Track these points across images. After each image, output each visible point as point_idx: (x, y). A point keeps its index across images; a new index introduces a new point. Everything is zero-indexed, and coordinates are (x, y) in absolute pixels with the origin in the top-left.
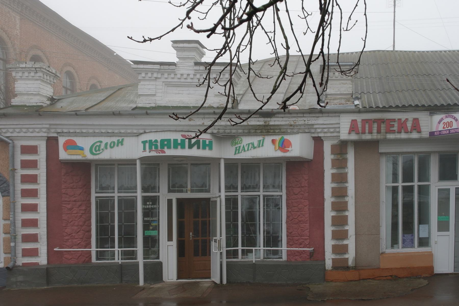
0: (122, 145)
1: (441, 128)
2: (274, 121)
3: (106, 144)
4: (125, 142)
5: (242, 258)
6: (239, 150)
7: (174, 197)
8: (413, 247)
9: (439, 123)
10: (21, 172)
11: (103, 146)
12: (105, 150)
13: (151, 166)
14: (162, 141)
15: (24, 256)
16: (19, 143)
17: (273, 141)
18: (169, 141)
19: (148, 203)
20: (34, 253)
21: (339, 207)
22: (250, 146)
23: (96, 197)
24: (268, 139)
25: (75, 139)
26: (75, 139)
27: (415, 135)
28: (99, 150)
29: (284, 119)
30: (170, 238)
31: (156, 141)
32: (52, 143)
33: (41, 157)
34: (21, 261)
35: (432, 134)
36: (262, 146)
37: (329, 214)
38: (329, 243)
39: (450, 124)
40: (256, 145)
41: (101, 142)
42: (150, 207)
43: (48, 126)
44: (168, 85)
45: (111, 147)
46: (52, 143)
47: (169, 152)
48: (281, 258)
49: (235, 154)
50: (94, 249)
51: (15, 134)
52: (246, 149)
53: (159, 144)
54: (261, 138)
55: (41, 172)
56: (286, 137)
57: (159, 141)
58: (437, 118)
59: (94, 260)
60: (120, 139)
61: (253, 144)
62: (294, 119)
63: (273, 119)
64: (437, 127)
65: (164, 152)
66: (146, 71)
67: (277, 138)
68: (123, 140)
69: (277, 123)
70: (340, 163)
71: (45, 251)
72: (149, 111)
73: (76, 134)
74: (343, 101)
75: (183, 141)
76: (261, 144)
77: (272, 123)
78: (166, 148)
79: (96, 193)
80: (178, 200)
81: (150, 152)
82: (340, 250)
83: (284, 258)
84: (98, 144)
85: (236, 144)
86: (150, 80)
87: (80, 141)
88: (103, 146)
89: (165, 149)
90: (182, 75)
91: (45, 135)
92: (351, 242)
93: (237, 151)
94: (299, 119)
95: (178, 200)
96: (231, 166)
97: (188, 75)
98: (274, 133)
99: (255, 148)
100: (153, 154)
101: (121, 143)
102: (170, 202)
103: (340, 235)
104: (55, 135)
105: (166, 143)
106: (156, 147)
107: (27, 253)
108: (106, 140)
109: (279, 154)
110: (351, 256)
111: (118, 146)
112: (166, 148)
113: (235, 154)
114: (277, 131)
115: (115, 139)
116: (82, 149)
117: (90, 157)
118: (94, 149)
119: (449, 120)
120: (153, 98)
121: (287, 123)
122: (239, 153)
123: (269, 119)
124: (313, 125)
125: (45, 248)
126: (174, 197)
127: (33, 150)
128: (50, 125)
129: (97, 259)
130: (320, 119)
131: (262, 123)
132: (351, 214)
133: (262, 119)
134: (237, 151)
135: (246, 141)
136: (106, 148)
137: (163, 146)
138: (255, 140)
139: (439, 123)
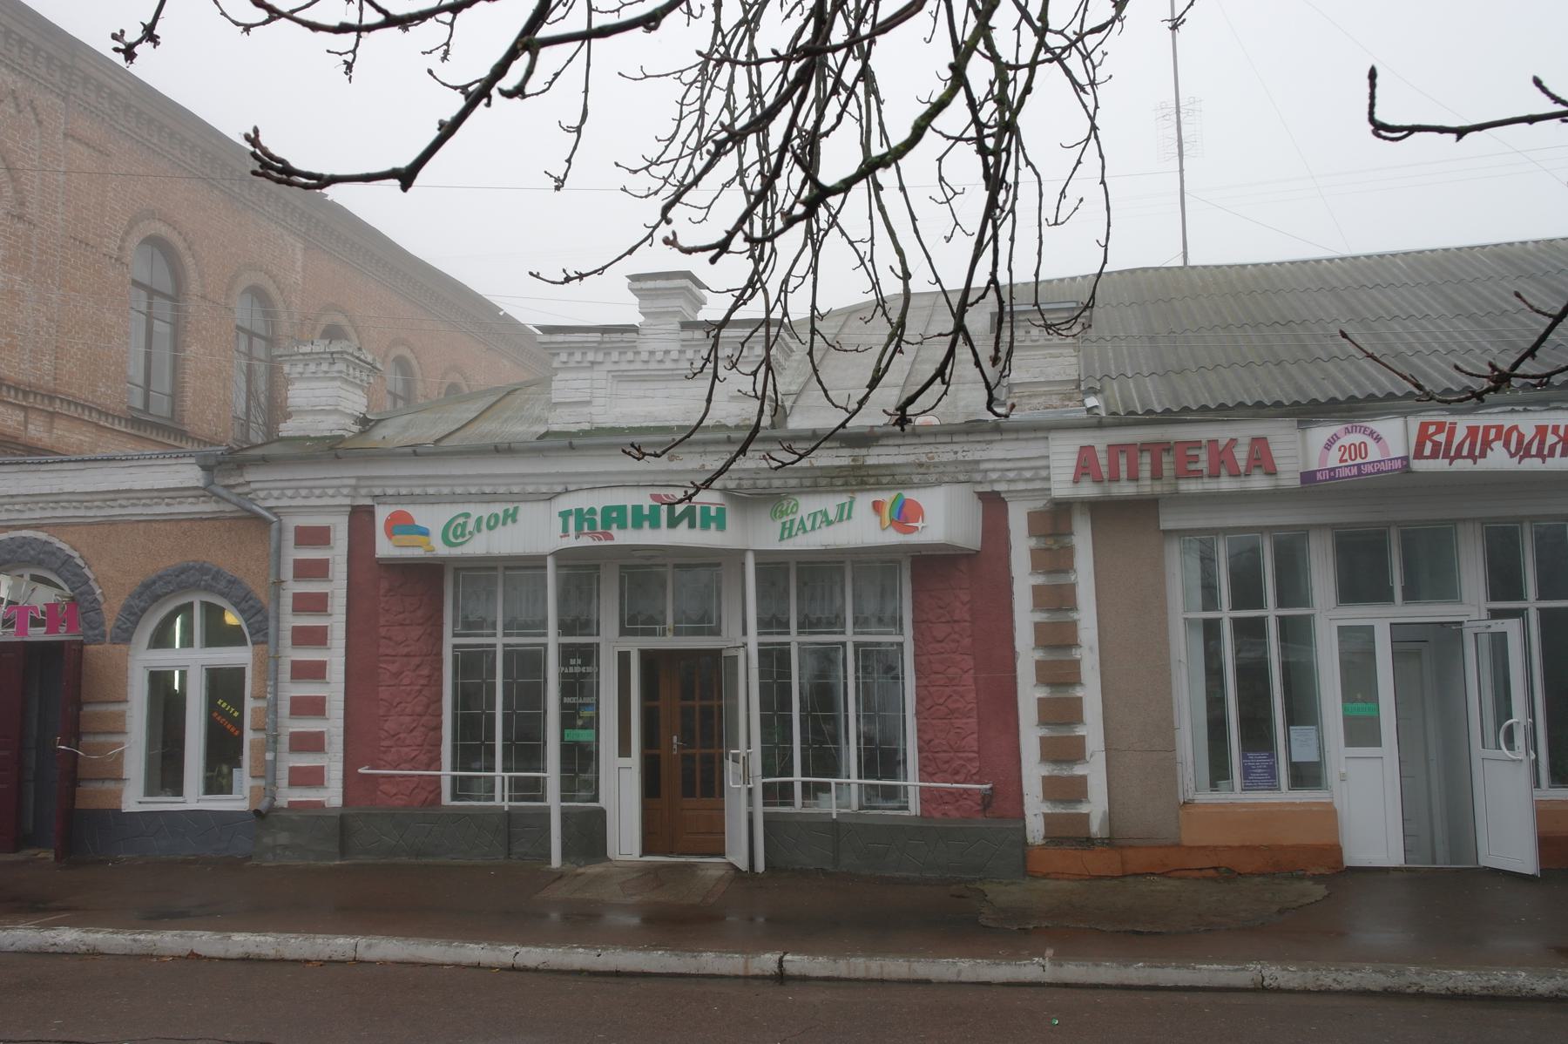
0: (514, 521)
1: (1333, 460)
2: (876, 457)
3: (479, 520)
4: (520, 516)
5: (804, 806)
6: (791, 529)
7: (635, 645)
8: (1274, 786)
9: (1328, 446)
10: (294, 587)
11: (471, 526)
12: (477, 536)
13: (580, 571)
14: (607, 510)
15: (293, 783)
16: (293, 522)
17: (877, 506)
18: (622, 509)
19: (572, 662)
20: (313, 777)
21: (1060, 675)
22: (819, 518)
23: (455, 646)
24: (863, 502)
25: (410, 509)
26: (410, 509)
27: (1259, 482)
28: (463, 535)
29: (903, 450)
30: (624, 751)
31: (592, 511)
32: (361, 518)
33: (337, 553)
34: (288, 795)
35: (1308, 477)
36: (849, 517)
37: (1029, 694)
38: (1033, 772)
39: (1360, 450)
40: (832, 517)
41: (467, 515)
42: (577, 670)
43: (353, 482)
44: (621, 377)
45: (490, 528)
46: (361, 518)
47: (624, 537)
48: (906, 808)
49: (782, 539)
50: (446, 773)
51: (284, 502)
52: (808, 525)
53: (598, 519)
54: (844, 499)
55: (336, 587)
56: (909, 494)
57: (599, 510)
58: (1320, 434)
59: (446, 799)
60: (511, 507)
61: (825, 514)
62: (927, 449)
63: (874, 451)
64: (1323, 459)
65: (612, 538)
66: (571, 349)
67: (887, 497)
68: (516, 509)
69: (884, 460)
70: (1053, 558)
71: (340, 774)
72: (576, 442)
73: (413, 499)
74: (1055, 401)
75: (655, 510)
76: (844, 514)
77: (870, 461)
78: (614, 526)
79: (455, 635)
80: (645, 655)
81: (577, 537)
82: (1066, 790)
83: (914, 807)
84: (461, 520)
85: (783, 513)
86: (579, 367)
87: (422, 515)
88: (471, 526)
89: (614, 531)
90: (652, 353)
91: (348, 501)
92: (1094, 771)
93: (787, 532)
94: (942, 448)
95: (645, 655)
96: (773, 569)
97: (667, 352)
98: (879, 486)
99: (830, 523)
100: (586, 541)
101: (512, 517)
102: (624, 658)
103: (1063, 750)
104: (368, 502)
105: (615, 516)
106: (593, 526)
107: (303, 777)
108: (478, 511)
109: (893, 537)
110: (1096, 807)
111: (504, 524)
112: (614, 526)
113: (782, 539)
114: (885, 480)
115: (498, 509)
116: (425, 533)
117: (442, 551)
118: (452, 532)
119: (1356, 438)
120: (586, 410)
121: (911, 458)
122: (790, 536)
123: (863, 451)
124: (977, 462)
125: (340, 766)
126: (635, 645)
127: (319, 536)
128: (358, 478)
129: (455, 797)
130: (996, 446)
131: (846, 461)
132: (1090, 693)
133: (846, 452)
134: (787, 532)
135: (808, 506)
136: (479, 530)
137: (607, 524)
138: (830, 503)
139: (1328, 446)
